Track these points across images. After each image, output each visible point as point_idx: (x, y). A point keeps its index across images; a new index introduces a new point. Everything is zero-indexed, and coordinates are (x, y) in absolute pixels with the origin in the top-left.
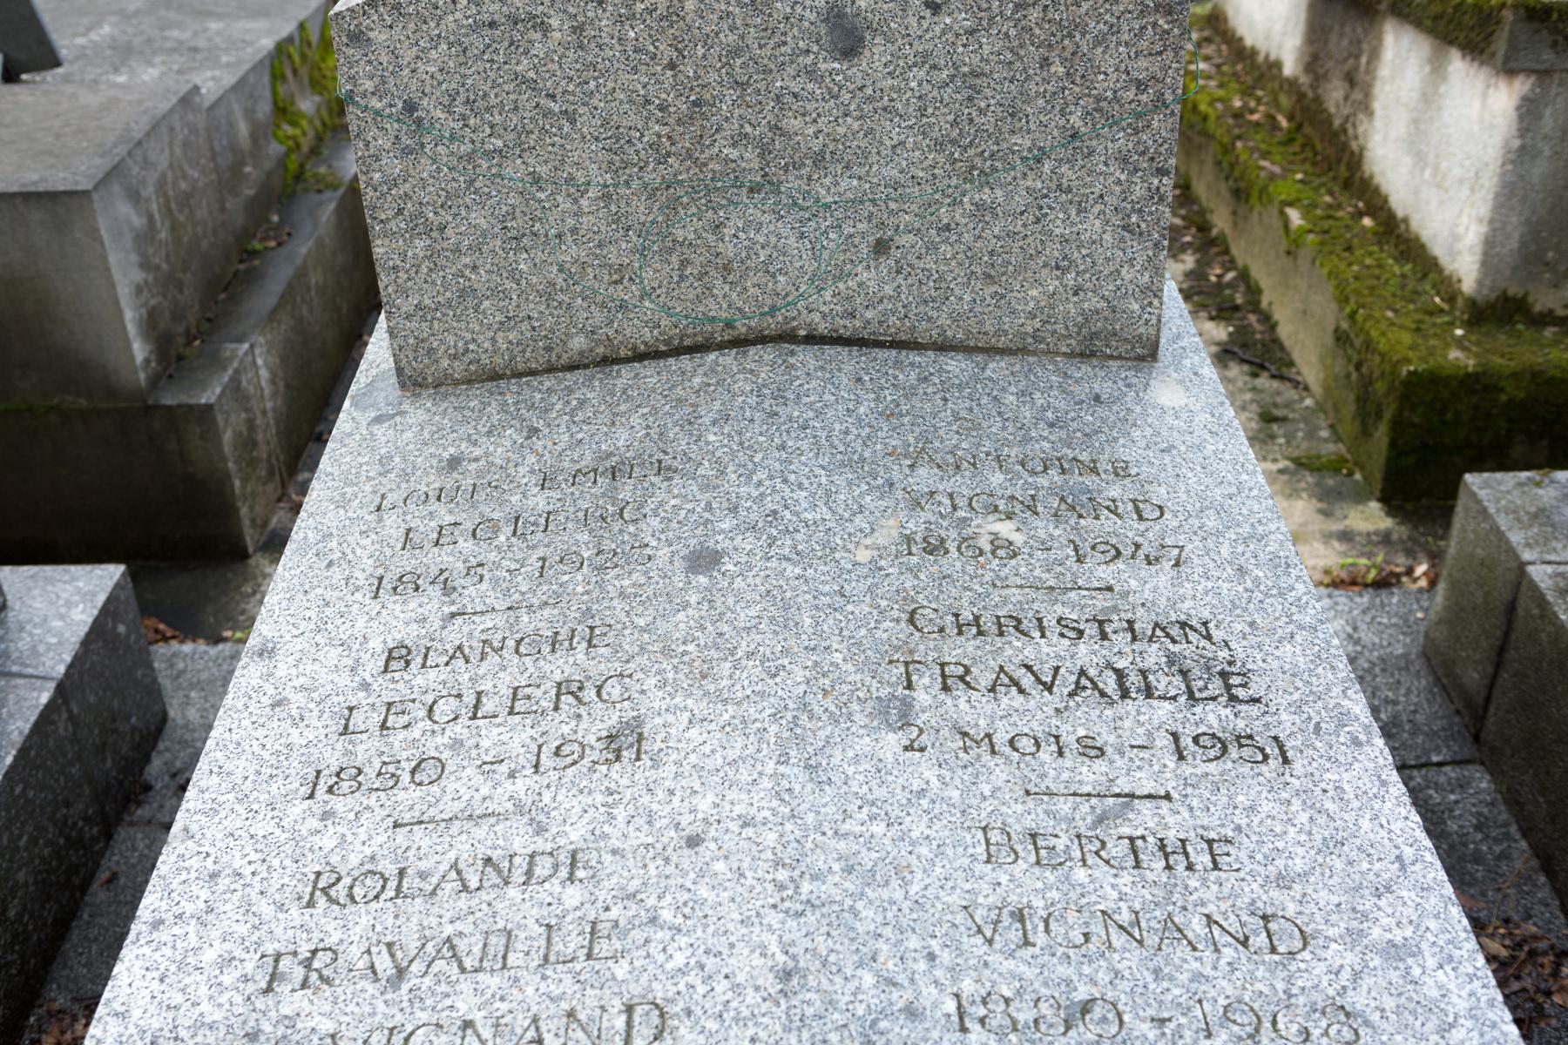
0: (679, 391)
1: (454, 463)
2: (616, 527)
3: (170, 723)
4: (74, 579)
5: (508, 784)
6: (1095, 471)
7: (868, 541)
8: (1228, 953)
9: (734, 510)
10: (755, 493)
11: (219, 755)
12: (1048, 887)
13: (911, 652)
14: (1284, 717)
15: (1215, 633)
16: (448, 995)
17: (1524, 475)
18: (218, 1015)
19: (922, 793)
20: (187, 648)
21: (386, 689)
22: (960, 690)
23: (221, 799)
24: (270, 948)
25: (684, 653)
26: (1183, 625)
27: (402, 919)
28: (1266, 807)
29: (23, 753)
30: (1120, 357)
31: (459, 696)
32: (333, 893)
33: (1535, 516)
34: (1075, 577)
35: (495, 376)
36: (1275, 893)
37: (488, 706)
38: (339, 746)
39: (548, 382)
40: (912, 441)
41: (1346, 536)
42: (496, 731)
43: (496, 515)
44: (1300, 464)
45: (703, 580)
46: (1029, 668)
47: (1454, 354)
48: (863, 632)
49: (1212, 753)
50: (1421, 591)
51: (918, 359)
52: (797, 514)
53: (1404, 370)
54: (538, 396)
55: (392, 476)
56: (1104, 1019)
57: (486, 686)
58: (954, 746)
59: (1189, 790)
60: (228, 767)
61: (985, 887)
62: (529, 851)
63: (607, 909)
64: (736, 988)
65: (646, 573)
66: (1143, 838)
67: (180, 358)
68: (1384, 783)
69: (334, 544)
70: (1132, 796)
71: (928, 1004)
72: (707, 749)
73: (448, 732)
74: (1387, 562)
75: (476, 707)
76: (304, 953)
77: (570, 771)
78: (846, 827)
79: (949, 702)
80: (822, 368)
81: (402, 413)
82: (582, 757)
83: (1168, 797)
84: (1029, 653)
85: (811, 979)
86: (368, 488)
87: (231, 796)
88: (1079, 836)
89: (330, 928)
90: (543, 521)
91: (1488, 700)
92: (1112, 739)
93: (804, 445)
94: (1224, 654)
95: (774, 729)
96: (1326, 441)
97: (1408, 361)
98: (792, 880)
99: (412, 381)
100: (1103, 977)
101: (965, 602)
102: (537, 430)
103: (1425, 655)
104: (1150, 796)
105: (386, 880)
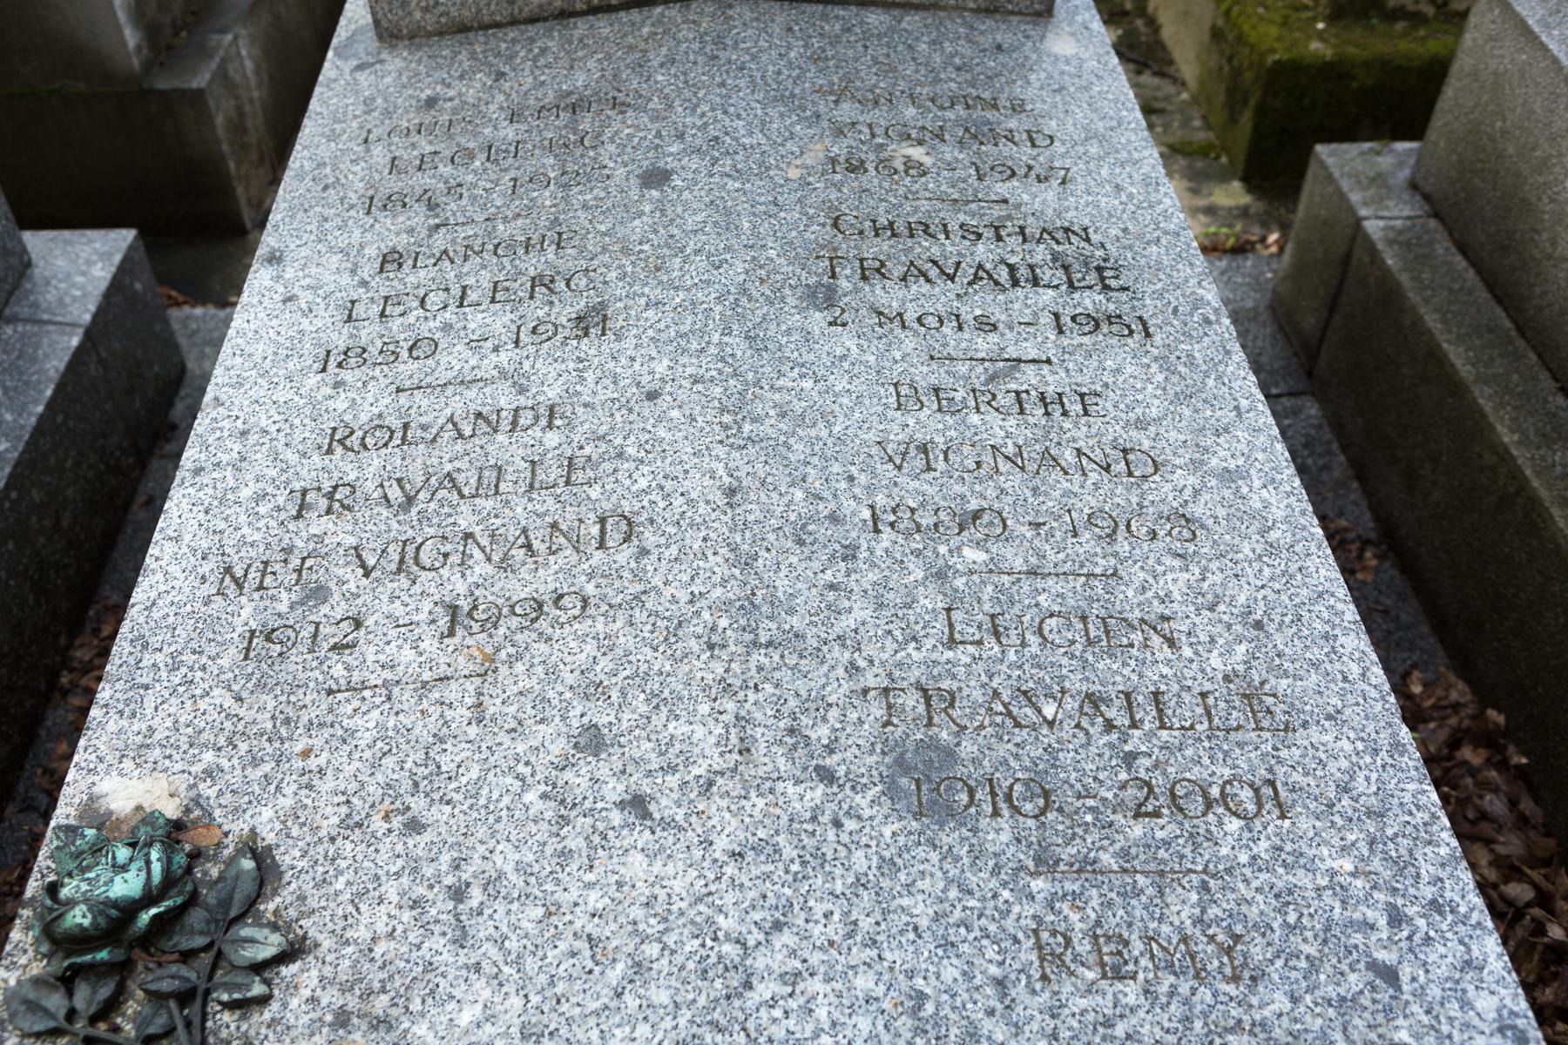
0: (630, 39)
1: (431, 102)
2: (578, 152)
3: (189, 374)
4: (91, 241)
5: (493, 356)
6: (995, 107)
7: (798, 162)
9: (681, 136)
10: (699, 123)
11: (240, 341)
12: (947, 428)
13: (835, 250)
14: (1148, 302)
15: (1093, 237)
16: (450, 515)
17: (1367, 145)
18: (257, 536)
19: (844, 357)
20: (199, 311)
21: (382, 287)
22: (876, 279)
23: (245, 375)
24: (297, 486)
25: (641, 251)
26: (1067, 230)
27: (408, 461)
28: (1129, 370)
29: (60, 388)
30: (1020, 13)
31: (447, 290)
32: (348, 443)
33: (1373, 180)
34: (976, 191)
35: (463, 29)
36: (1134, 433)
37: (473, 296)
38: (345, 331)
39: (512, 33)
40: (836, 80)
41: (1210, 211)
42: (480, 316)
43: (471, 145)
45: (655, 193)
46: (935, 263)
47: (1315, 45)
48: (794, 233)
49: (1087, 329)
50: (1272, 256)
51: (842, 13)
52: (736, 139)
53: (1270, 59)
54: (503, 46)
55: (376, 114)
56: (991, 523)
57: (471, 281)
58: (871, 322)
59: (1067, 356)
60: (248, 349)
61: (896, 428)
62: (513, 406)
63: (581, 448)
64: (691, 503)
65: (605, 189)
66: (1027, 392)
67: (169, 48)
68: (1228, 352)
69: (328, 170)
70: (1019, 360)
71: (848, 513)
72: (662, 325)
73: (439, 318)
74: (1245, 232)
75: (462, 298)
76: (327, 486)
77: (546, 345)
78: (780, 383)
79: (867, 288)
80: (757, 19)
81: (381, 62)
82: (555, 334)
83: (1048, 361)
84: (935, 251)
85: (753, 497)
86: (355, 124)
87: (254, 372)
88: (974, 391)
89: (347, 470)
90: (513, 149)
91: (1321, 341)
92: (1003, 317)
93: (742, 83)
94: (1099, 253)
95: (719, 308)
96: (1198, 129)
97: (1273, 51)
98: (735, 422)
99: (389, 33)
100: (991, 493)
101: (881, 210)
102: (503, 74)
103: (1272, 309)
104: (1034, 361)
105: (392, 432)
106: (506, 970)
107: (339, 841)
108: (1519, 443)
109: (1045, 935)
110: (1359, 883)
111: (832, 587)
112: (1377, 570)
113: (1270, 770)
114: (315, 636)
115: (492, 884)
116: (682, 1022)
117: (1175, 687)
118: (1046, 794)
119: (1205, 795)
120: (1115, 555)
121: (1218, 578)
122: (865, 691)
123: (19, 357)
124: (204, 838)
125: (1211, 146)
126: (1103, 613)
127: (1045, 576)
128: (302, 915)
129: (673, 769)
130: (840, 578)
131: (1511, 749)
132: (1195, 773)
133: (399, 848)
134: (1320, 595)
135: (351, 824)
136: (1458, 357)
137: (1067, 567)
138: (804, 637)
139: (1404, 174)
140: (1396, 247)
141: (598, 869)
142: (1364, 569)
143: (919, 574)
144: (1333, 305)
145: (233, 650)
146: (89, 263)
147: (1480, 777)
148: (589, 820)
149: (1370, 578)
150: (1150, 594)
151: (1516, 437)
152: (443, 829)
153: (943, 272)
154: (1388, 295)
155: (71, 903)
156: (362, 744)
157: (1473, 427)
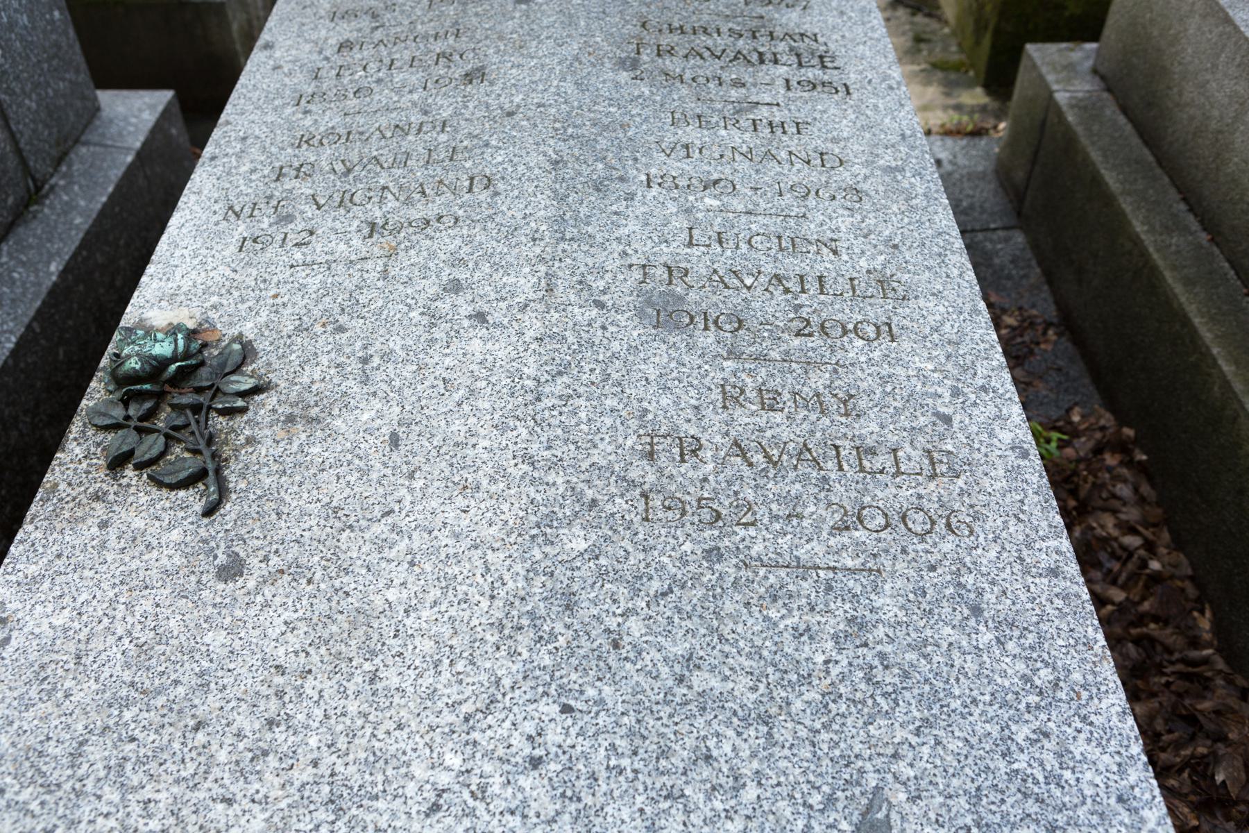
8: (798, 166)
11: (244, 91)
17: (1064, 45)
18: (250, 191)
19: (639, 97)
26: (802, 35)
28: (832, 111)
29: (118, 187)
33: (1065, 67)
36: (829, 145)
37: (397, 64)
44: (935, 66)
45: (524, 7)
46: (708, 49)
64: (530, 169)
70: (758, 103)
76: (296, 164)
83: (778, 105)
84: (710, 43)
91: (1027, 187)
94: (823, 48)
95: (559, 68)
100: (728, 170)
101: (676, 19)
103: (997, 172)
106: (392, 395)
107: (294, 338)
108: (1148, 231)
109: (728, 388)
110: (936, 375)
111: (616, 213)
112: (1055, 343)
113: (889, 318)
114: (284, 240)
115: (386, 356)
116: (496, 416)
117: (834, 274)
118: (740, 322)
119: (844, 327)
120: (806, 206)
121: (873, 222)
122: (630, 266)
123: (91, 166)
124: (210, 337)
125: (962, 64)
126: (792, 235)
127: (756, 215)
128: (269, 372)
129: (504, 299)
130: (622, 209)
131: (1137, 451)
132: (840, 316)
133: (331, 340)
134: (940, 234)
135: (299, 330)
136: (1111, 179)
137: (773, 211)
138: (594, 237)
139: (1089, 64)
140: (1076, 110)
141: (453, 347)
142: (1046, 341)
143: (675, 210)
144: (1034, 161)
145: (232, 247)
146: (140, 110)
147: (1115, 472)
148: (449, 325)
149: (1049, 347)
150: (825, 227)
151: (1146, 228)
152: (358, 331)
153: (713, 54)
154: (1069, 141)
155: (129, 357)
156: (311, 291)
157: (1118, 224)
